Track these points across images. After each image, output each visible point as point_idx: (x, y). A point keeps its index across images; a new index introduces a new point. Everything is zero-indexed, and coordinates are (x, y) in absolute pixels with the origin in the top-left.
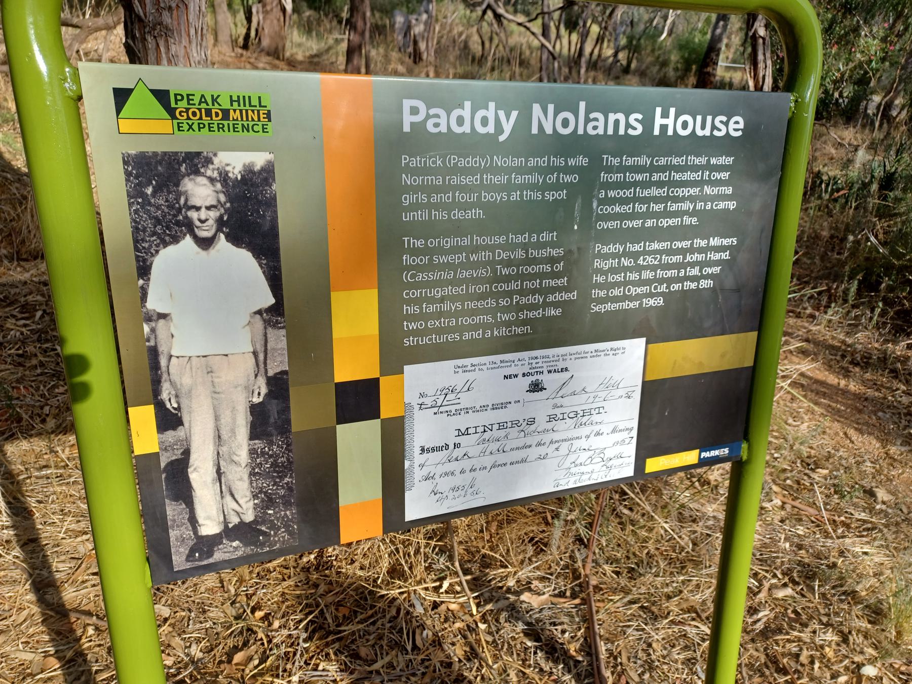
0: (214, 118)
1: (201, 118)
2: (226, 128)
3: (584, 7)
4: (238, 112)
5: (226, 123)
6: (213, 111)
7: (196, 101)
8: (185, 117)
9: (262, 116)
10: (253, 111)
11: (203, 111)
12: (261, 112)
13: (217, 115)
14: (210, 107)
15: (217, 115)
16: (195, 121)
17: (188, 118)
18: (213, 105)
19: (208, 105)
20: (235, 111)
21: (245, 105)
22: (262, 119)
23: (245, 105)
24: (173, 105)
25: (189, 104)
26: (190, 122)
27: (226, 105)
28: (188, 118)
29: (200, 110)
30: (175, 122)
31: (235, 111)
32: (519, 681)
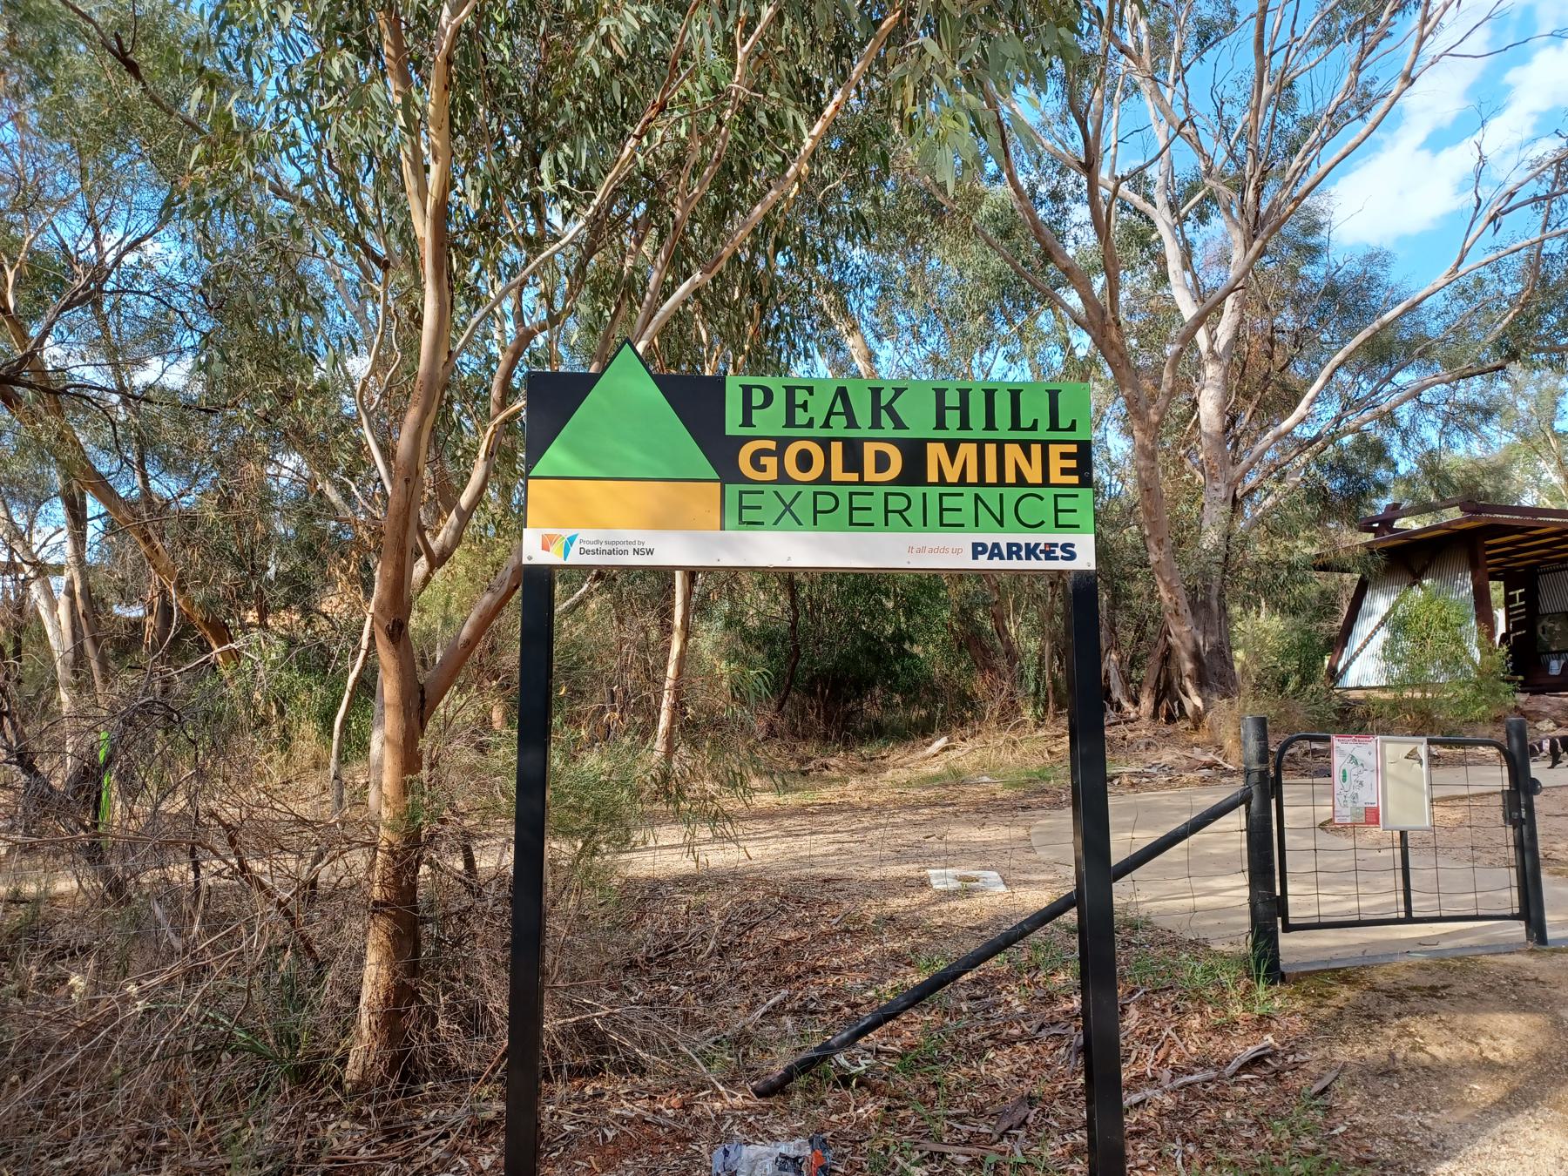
0: (870, 474)
1: (825, 478)
2: (914, 514)
3: (1109, 22)
4: (968, 452)
5: (915, 492)
6: (869, 451)
7: (818, 410)
8: (771, 473)
9: (1056, 464)
10: (1025, 446)
11: (837, 449)
12: (1055, 451)
13: (882, 462)
14: (864, 430)
15: (882, 462)
16: (966, 500)
17: (783, 478)
18: (876, 424)
19: (852, 423)
20: (952, 447)
21: (990, 425)
22: (1056, 477)
23: (990, 425)
24: (733, 426)
25: (790, 423)
26: (788, 492)
27: (919, 424)
28: (783, 478)
29: (825, 444)
30: (733, 490)
31: (952, 447)
32: (438, 5)
